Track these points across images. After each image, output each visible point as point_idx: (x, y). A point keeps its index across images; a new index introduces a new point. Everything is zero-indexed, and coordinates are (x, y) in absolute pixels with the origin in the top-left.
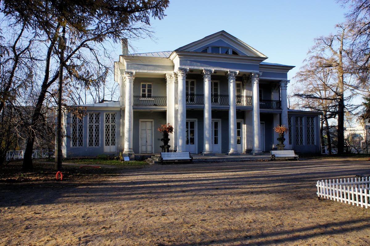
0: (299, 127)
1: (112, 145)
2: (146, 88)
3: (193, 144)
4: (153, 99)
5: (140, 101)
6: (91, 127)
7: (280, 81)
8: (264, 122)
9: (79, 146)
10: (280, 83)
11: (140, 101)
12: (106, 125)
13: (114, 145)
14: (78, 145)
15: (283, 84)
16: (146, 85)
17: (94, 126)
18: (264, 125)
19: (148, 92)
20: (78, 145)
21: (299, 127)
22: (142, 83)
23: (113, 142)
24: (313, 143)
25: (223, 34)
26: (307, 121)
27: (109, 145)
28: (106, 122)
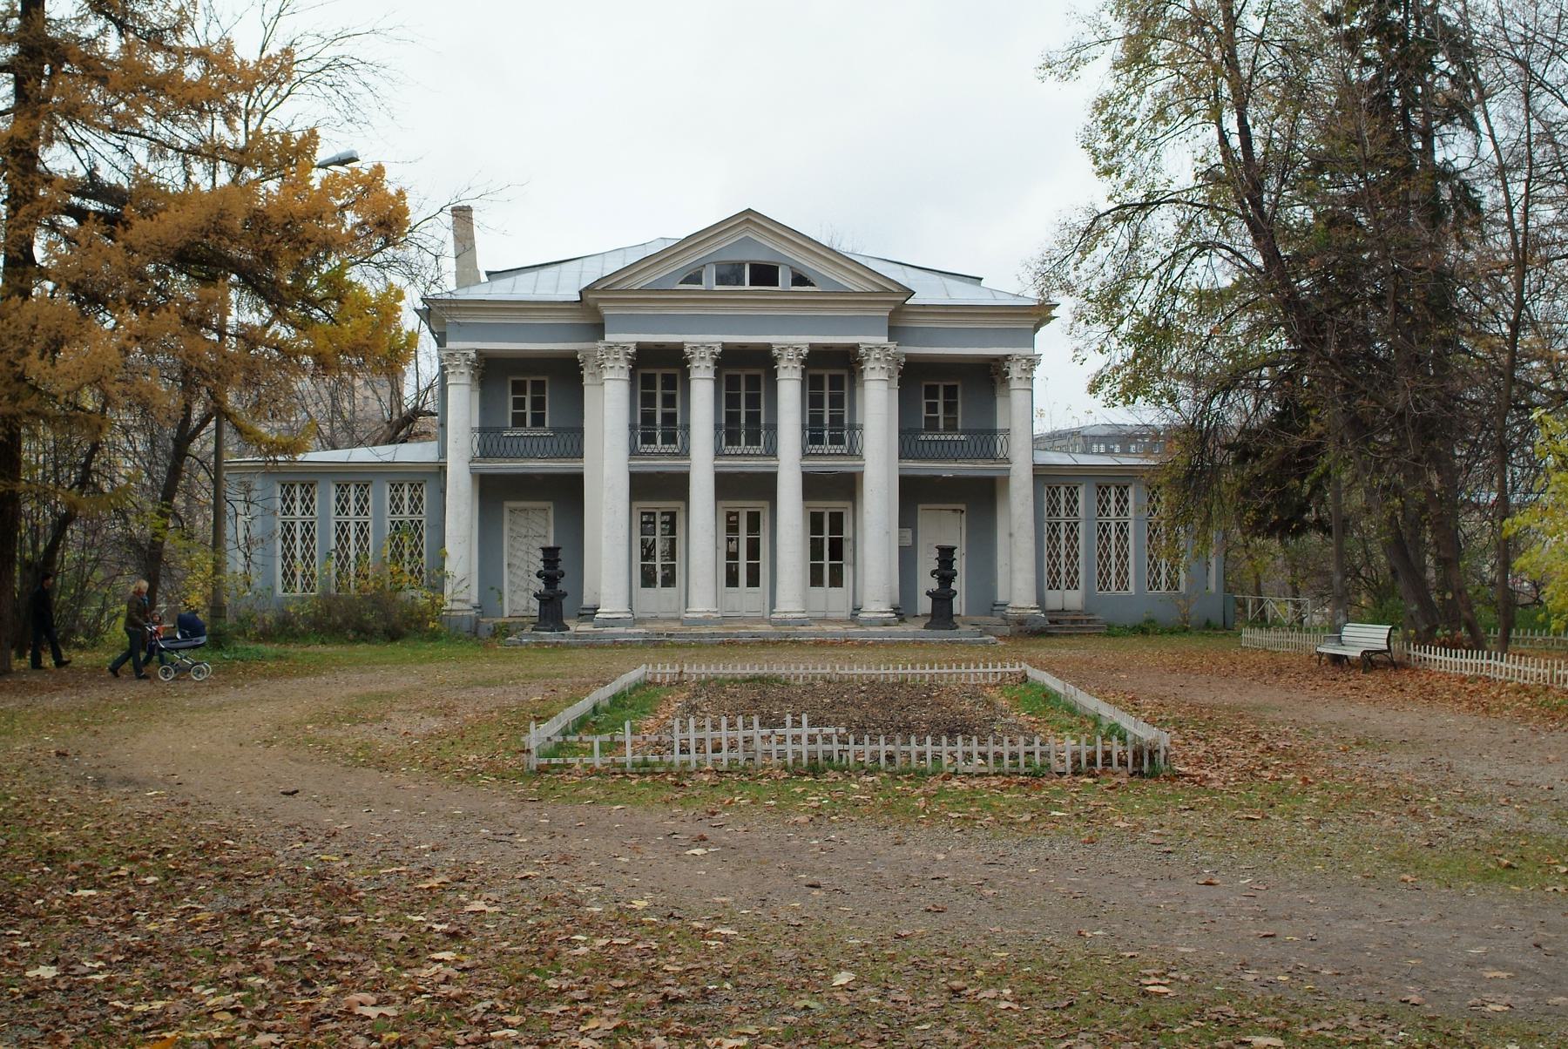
0: (1113, 524)
1: (1068, 588)
2: (937, 398)
3: (757, 585)
4: (962, 437)
5: (920, 445)
6: (343, 530)
7: (1006, 357)
8: (963, 507)
9: (304, 591)
10: (1006, 364)
11: (920, 445)
12: (393, 522)
13: (1076, 588)
14: (1113, 588)
15: (1015, 371)
16: (525, 382)
17: (352, 525)
18: (964, 516)
19: (533, 408)
20: (1113, 588)
21: (1113, 524)
22: (511, 379)
23: (1072, 580)
24: (1173, 584)
25: (749, 217)
26: (1100, 501)
27: (1058, 588)
28: (393, 513)
